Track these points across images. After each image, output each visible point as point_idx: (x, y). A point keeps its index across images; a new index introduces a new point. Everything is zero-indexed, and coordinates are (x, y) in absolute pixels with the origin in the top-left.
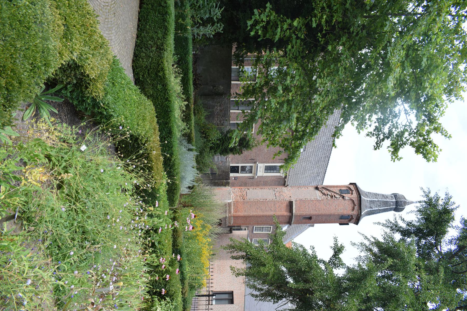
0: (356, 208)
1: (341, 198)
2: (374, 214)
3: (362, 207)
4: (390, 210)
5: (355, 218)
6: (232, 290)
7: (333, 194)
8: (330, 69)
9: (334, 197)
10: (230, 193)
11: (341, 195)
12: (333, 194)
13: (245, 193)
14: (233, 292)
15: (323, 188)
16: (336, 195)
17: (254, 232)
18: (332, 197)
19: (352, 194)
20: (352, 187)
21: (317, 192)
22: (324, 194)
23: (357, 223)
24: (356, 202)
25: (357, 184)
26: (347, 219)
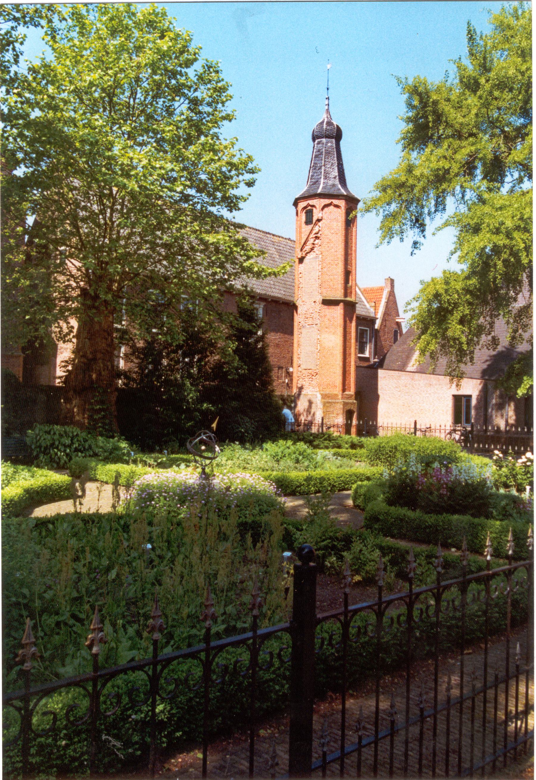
1: (320, 224)
7: (312, 235)
9: (318, 235)
11: (316, 224)
12: (312, 235)
15: (301, 250)
16: (314, 232)
18: (317, 238)
19: (313, 206)
20: (302, 205)
21: (306, 261)
22: (312, 249)
24: (327, 201)
25: (297, 196)
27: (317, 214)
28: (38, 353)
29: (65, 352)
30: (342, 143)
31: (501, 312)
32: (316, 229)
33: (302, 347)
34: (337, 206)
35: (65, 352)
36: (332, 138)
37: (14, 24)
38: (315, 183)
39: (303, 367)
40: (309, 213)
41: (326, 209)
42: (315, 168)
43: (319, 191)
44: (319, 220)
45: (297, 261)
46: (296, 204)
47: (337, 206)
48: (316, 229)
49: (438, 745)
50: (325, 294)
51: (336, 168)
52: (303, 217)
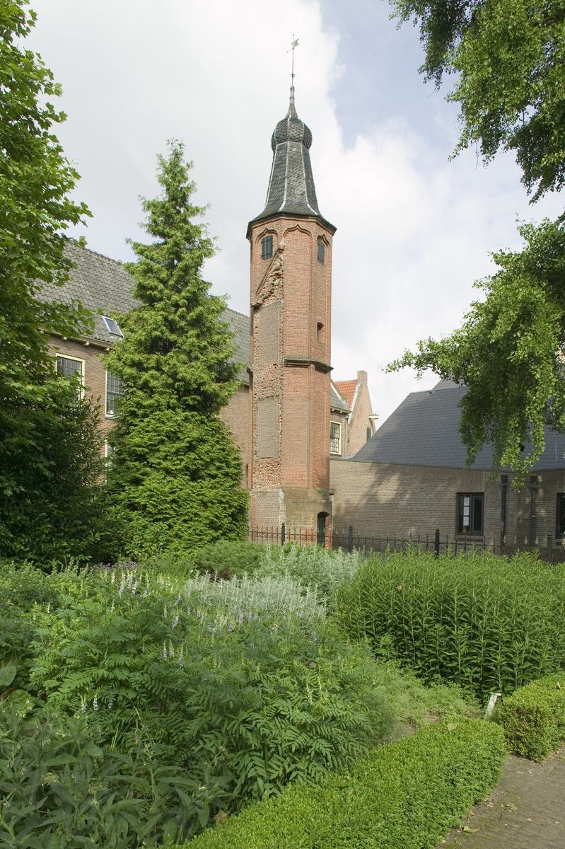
0: (303, 224)
1: (281, 256)
2: (314, 192)
3: (302, 212)
4: (307, 156)
5: (323, 232)
6: (455, 495)
8: (52, 538)
9: (280, 272)
10: (264, 493)
13: (264, 461)
14: (457, 493)
16: (274, 267)
17: (340, 453)
19: (273, 232)
20: (257, 231)
23: (332, 229)
25: (251, 219)
26: (323, 247)
28: (460, 518)
30: (311, 151)
34: (303, 231)
36: (299, 141)
38: (275, 201)
40: (267, 242)
41: (290, 235)
43: (281, 209)
44: (280, 250)
46: (249, 235)
47: (303, 231)
49: (314, 251)
50: (288, 354)
51: (304, 182)
52: (259, 250)
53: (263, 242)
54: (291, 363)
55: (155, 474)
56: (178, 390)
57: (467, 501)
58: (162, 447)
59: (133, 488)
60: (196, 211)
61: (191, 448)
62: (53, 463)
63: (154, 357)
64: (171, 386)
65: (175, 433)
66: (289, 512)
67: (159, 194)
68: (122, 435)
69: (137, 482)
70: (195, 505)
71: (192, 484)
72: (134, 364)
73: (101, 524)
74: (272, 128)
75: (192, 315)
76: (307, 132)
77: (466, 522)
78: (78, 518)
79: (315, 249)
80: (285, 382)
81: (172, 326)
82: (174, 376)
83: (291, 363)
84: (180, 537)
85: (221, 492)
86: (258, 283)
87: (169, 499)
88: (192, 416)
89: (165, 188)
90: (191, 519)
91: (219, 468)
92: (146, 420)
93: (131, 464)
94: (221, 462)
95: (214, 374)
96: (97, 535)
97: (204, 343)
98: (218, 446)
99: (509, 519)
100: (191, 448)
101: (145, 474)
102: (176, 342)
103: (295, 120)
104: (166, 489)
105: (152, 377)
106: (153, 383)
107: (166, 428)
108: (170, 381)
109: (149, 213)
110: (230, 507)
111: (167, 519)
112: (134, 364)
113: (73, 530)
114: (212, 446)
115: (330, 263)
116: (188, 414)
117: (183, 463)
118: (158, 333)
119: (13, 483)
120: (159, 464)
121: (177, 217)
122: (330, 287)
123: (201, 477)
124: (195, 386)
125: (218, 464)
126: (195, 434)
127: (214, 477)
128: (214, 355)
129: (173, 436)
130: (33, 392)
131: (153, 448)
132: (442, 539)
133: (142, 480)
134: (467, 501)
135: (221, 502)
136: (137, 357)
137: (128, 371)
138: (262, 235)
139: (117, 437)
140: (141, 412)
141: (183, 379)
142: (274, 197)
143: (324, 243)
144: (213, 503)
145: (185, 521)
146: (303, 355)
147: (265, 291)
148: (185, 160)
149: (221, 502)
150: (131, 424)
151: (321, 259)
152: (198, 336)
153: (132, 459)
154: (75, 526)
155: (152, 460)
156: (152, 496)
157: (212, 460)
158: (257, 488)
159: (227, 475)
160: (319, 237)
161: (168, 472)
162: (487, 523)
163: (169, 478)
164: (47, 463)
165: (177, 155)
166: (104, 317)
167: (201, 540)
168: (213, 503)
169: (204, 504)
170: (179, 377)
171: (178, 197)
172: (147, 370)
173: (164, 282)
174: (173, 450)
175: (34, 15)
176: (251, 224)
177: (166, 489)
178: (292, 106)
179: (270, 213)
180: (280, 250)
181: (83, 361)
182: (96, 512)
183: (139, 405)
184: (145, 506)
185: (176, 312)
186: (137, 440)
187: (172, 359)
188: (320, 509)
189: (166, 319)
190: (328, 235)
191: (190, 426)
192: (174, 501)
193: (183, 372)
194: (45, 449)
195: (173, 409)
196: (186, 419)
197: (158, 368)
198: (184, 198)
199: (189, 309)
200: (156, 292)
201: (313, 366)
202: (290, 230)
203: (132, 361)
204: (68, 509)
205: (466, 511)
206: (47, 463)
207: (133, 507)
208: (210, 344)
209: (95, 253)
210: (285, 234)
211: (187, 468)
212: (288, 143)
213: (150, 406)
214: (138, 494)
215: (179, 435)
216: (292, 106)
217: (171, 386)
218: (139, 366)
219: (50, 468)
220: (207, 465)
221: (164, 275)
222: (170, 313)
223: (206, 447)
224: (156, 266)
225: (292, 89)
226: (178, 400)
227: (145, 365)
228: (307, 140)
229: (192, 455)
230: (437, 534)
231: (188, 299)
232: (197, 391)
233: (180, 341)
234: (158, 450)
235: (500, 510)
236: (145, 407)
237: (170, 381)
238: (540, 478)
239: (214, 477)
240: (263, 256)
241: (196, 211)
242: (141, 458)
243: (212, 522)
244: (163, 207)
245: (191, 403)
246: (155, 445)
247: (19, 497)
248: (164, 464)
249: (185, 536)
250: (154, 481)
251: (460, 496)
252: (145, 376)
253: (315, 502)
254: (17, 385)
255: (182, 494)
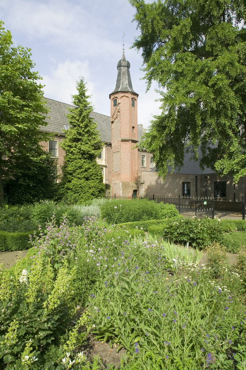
0: (126, 95)
1: (120, 105)
2: (131, 83)
5: (133, 96)
9: (119, 111)
10: (116, 184)
12: (117, 111)
16: (117, 109)
19: (117, 97)
20: (112, 97)
23: (137, 95)
24: (123, 95)
25: (110, 94)
27: (119, 101)
29: (176, 191)
30: (130, 69)
31: (17, 205)
32: (118, 108)
33: (114, 162)
34: (127, 97)
35: (176, 191)
37: (243, 353)
39: (114, 171)
41: (122, 98)
42: (118, 81)
43: (119, 90)
44: (119, 104)
45: (111, 123)
47: (127, 97)
48: (118, 108)
52: (113, 104)
53: (114, 101)
54: (123, 141)
55: (75, 179)
56: (81, 153)
57: (186, 185)
58: (77, 171)
59: (69, 184)
60: (88, 97)
61: (86, 171)
62: (43, 177)
63: (74, 143)
64: (79, 152)
65: (81, 166)
66: (123, 190)
67: (77, 93)
68: (66, 168)
69: (70, 182)
70: (87, 188)
71: (86, 182)
72: (68, 146)
73: (57, 194)
74: (117, 64)
75: (86, 130)
76: (128, 63)
77: (186, 192)
78: (51, 193)
79: (131, 102)
80: (121, 147)
81: (80, 134)
82: (80, 149)
83: (123, 141)
84: (83, 198)
85: (95, 184)
86: (113, 114)
87: (79, 186)
88: (87, 161)
89: (78, 91)
90: (86, 193)
91: (95, 177)
92: (72, 163)
93: (68, 176)
94: (95, 175)
95: (93, 148)
96: (56, 197)
97: (90, 138)
98: (94, 170)
99: (198, 191)
100: (86, 171)
101: (72, 179)
102: (81, 138)
103: (124, 60)
104: (78, 184)
105: (74, 150)
106: (74, 152)
107: (78, 165)
108: (79, 151)
109: (74, 99)
110: (98, 188)
111: (79, 192)
112: (68, 146)
113: (49, 196)
114: (93, 170)
115: (137, 106)
116: (85, 160)
117: (83, 176)
118: (75, 137)
119: (33, 183)
120: (76, 176)
121: (82, 100)
122: (137, 114)
123: (89, 180)
124: (86, 152)
125: (94, 175)
126: (87, 167)
127: (93, 179)
128: (93, 142)
129: (80, 167)
130: (36, 160)
131: (74, 171)
132: (155, 197)
133: (71, 181)
134: (186, 185)
135: (95, 187)
136: (70, 144)
137: (67, 148)
138: (113, 98)
139: (64, 167)
140: (71, 160)
141: (83, 150)
142: (118, 86)
143: (134, 100)
144: (93, 188)
145: (84, 193)
146: (127, 138)
147: (115, 117)
148: (84, 82)
149: (95, 187)
150: (68, 164)
151: (133, 105)
152: (88, 136)
153: (67, 176)
154: (50, 195)
155: (74, 175)
156: (74, 186)
157: (93, 174)
158: (113, 182)
159: (97, 179)
160: (132, 98)
161: (79, 178)
162: (191, 193)
163: (79, 180)
164: (42, 177)
165: (82, 81)
166: (65, 125)
167: (89, 199)
168: (93, 188)
169: (90, 188)
170: (82, 149)
171: (82, 94)
172: (73, 147)
173: (78, 120)
174: (80, 172)
175: (35, 64)
176: (110, 95)
177: (78, 184)
178: (124, 55)
179: (116, 91)
180: (119, 104)
181: (58, 141)
182: (56, 190)
183: (70, 158)
184: (72, 189)
185: (81, 129)
186: (69, 169)
187: (79, 144)
188: (135, 189)
189: (78, 132)
190: (136, 97)
191: (86, 164)
192: (80, 187)
193: (83, 148)
194: (41, 173)
195: (80, 159)
196: (84, 162)
197: (76, 147)
198: (84, 94)
199: (85, 129)
200: (75, 124)
201: (130, 141)
202: (122, 97)
203: (68, 145)
204: (48, 190)
205: (186, 189)
206: (42, 177)
207: (69, 189)
208: (92, 138)
209: (63, 103)
210: (121, 98)
211: (85, 177)
212: (122, 68)
213: (73, 158)
214: (70, 185)
215: (82, 167)
216: (124, 55)
217: (79, 152)
218: (70, 146)
219: (43, 178)
220: (91, 176)
221: (77, 118)
222: (79, 130)
223: (91, 170)
224: (75, 116)
225: (124, 49)
226: (82, 156)
227: (72, 146)
228: (128, 66)
229: (86, 173)
230: (154, 196)
231: (85, 125)
232: (87, 154)
233: (83, 138)
234: (76, 172)
235: (195, 188)
236: (72, 159)
237: (79, 151)
238: (208, 177)
239: (93, 179)
240: (114, 106)
241: (88, 97)
242: (71, 174)
243: (92, 193)
244: (77, 98)
245: (86, 157)
246: (75, 170)
247: (34, 187)
248: (78, 176)
249: (84, 198)
250: (75, 181)
251: (183, 183)
252: (72, 149)
253: (132, 186)
254: (32, 158)
255: (83, 185)
